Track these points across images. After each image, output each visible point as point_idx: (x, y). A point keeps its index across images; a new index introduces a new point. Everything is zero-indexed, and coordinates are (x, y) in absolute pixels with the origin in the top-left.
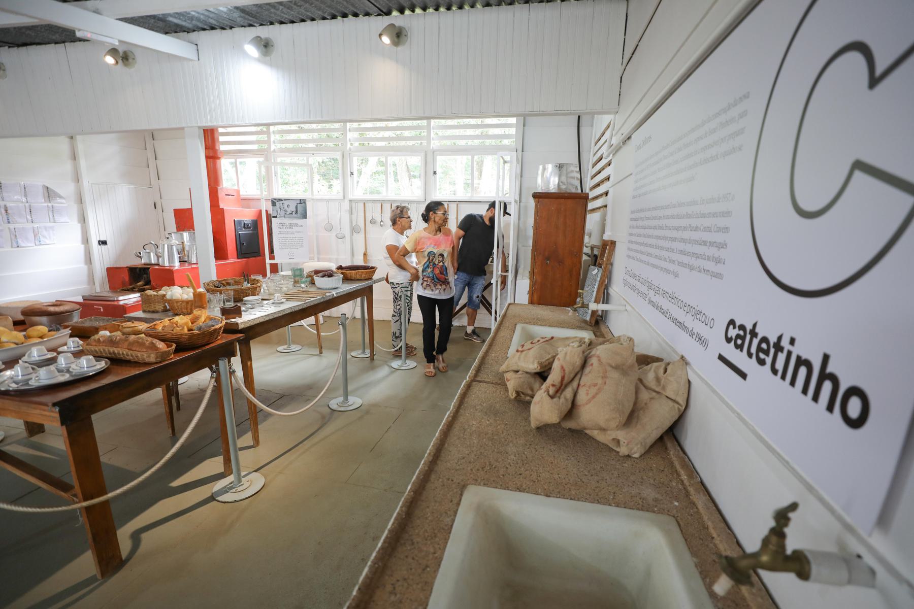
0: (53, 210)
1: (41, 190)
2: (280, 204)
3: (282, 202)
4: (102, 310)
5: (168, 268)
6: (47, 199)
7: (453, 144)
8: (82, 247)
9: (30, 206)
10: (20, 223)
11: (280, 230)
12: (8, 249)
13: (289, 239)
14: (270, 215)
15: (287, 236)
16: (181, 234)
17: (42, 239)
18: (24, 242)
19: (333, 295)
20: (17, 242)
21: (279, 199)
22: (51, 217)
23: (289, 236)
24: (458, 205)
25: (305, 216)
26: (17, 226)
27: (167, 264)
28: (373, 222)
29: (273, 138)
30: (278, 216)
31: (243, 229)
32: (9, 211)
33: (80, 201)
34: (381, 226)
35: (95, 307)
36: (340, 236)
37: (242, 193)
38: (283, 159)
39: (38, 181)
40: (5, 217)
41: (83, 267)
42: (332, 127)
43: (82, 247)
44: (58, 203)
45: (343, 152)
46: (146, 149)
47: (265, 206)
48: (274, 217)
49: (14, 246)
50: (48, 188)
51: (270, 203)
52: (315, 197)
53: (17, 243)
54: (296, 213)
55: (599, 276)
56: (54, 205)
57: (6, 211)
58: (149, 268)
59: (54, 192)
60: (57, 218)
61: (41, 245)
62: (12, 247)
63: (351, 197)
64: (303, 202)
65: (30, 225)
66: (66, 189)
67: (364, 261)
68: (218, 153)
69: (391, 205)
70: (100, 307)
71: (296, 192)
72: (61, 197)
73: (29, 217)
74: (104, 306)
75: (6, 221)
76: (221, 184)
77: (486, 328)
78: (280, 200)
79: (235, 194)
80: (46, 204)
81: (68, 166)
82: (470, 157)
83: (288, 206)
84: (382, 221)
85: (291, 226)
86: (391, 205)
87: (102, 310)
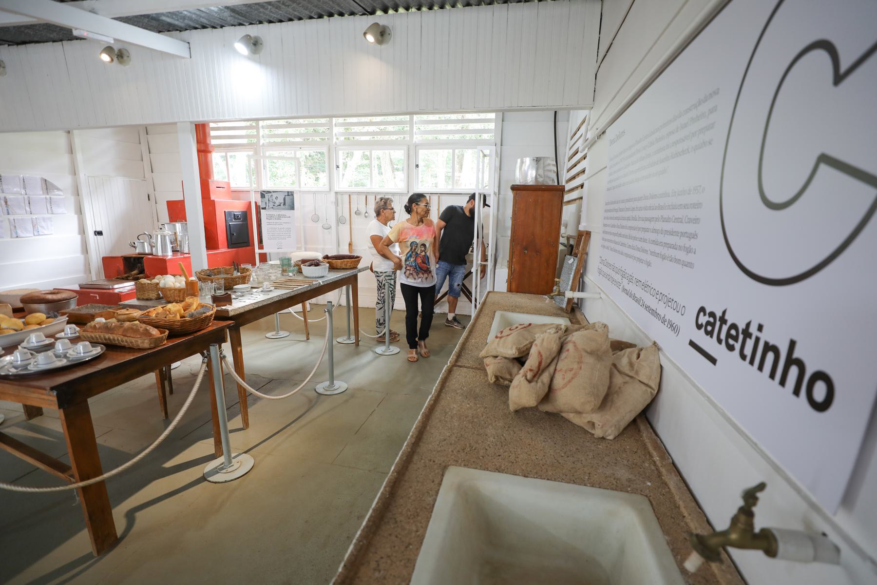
0: (50, 202)
1: (39, 183)
2: (268, 196)
3: (270, 194)
4: (98, 298)
5: (161, 257)
6: (45, 191)
8: (79, 237)
9: (29, 197)
10: (19, 214)
11: (268, 221)
13: (277, 229)
14: (259, 206)
15: (275, 226)
17: (40, 229)
18: (23, 233)
19: (320, 283)
20: (16, 233)
21: (268, 191)
22: (49, 208)
23: (277, 226)
24: (439, 197)
25: (292, 208)
26: (16, 217)
27: (160, 254)
28: (358, 213)
29: (262, 132)
31: (233, 220)
33: (77, 193)
34: (366, 217)
35: (91, 295)
36: (326, 226)
37: (232, 185)
38: (271, 152)
39: (36, 174)
40: (5, 209)
41: (80, 256)
43: (78, 238)
44: (56, 195)
45: (329, 146)
47: (254, 198)
48: (263, 208)
49: (13, 237)
50: (46, 180)
51: (259, 195)
52: (302, 189)
54: (284, 204)
55: (575, 265)
56: (52, 197)
57: (6, 202)
58: (143, 258)
59: (52, 185)
60: (55, 209)
61: (39, 235)
62: (11, 237)
63: (337, 189)
64: (290, 194)
65: (29, 217)
66: (64, 181)
67: (349, 251)
69: (376, 197)
70: (96, 295)
71: (284, 185)
72: (58, 189)
73: (28, 209)
75: (6, 212)
77: (466, 315)
78: (269, 192)
79: (225, 186)
80: (44, 196)
81: (65, 159)
82: (451, 151)
83: (276, 198)
84: (366, 212)
85: (279, 217)
86: (376, 197)
87: (98, 298)
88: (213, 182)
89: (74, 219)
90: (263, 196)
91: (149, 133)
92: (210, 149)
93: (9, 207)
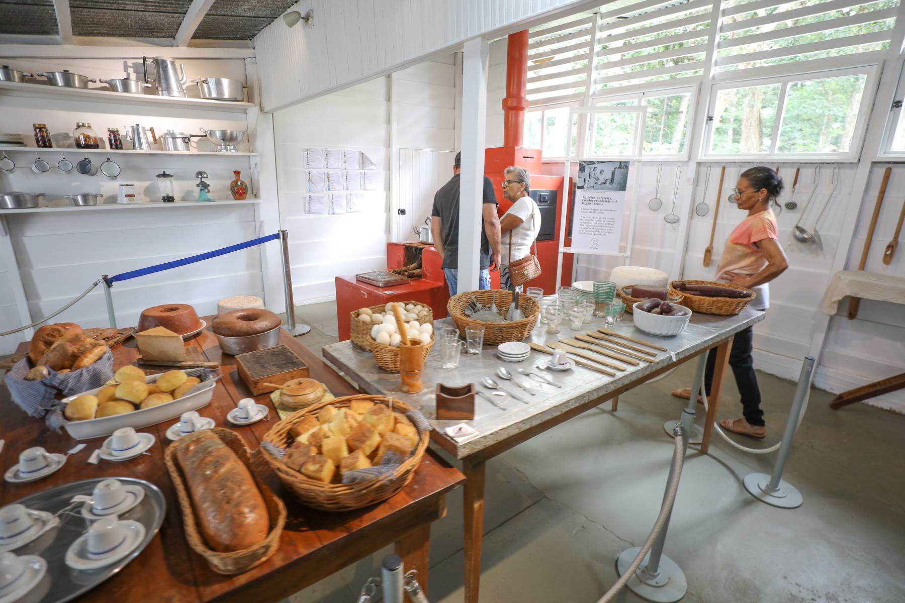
3: (593, 166)
6: (361, 165)
8: (385, 214)
9: (347, 172)
10: (338, 191)
11: (585, 206)
14: (575, 184)
15: (592, 215)
19: (671, 357)
21: (590, 162)
22: (362, 184)
25: (623, 187)
26: (352, 192)
30: (585, 186)
33: (388, 168)
36: (671, 218)
37: (543, 155)
39: (353, 148)
40: (327, 184)
42: (661, 79)
44: (370, 170)
45: (701, 83)
47: (570, 172)
48: (579, 188)
50: (363, 154)
51: (577, 168)
52: (644, 159)
54: (612, 181)
56: (366, 171)
62: (329, 214)
63: (701, 157)
64: (624, 166)
65: (345, 193)
66: (377, 156)
67: (705, 261)
71: (614, 153)
72: (372, 163)
73: (345, 184)
76: (520, 143)
78: (592, 163)
80: (359, 171)
81: (382, 131)
83: (601, 172)
85: (601, 201)
88: (520, 149)
89: (383, 194)
90: (582, 168)
92: (524, 104)
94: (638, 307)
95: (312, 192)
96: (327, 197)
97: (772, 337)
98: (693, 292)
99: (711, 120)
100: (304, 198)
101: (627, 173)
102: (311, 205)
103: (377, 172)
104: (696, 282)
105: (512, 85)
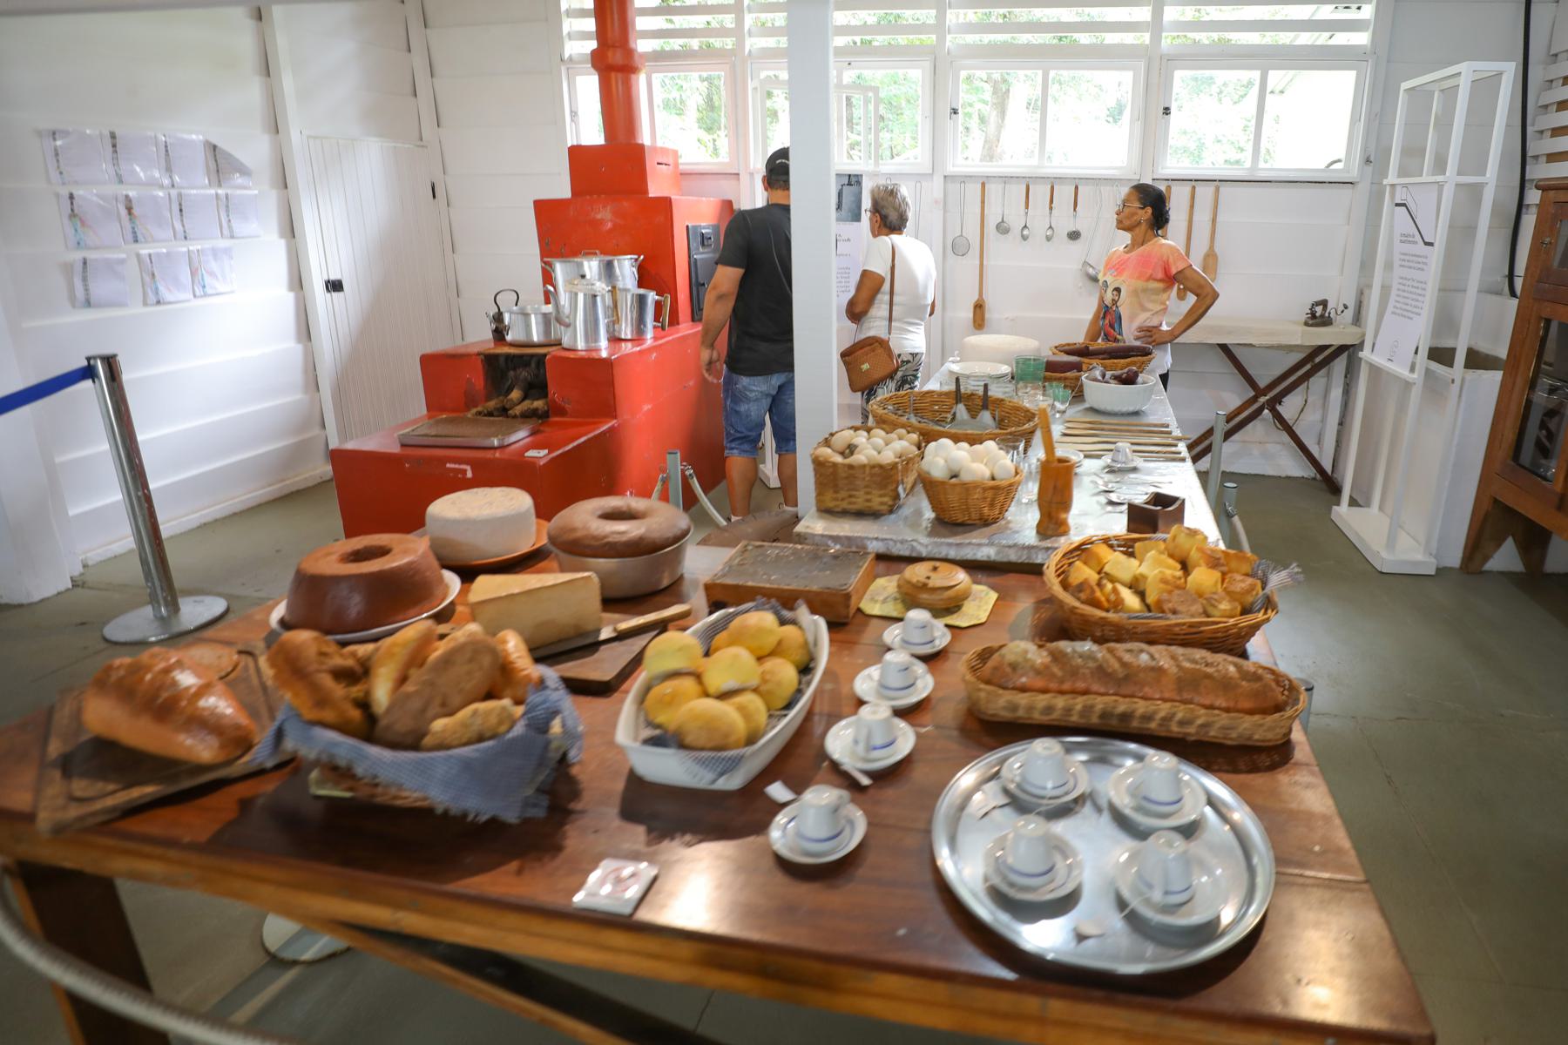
0: (227, 206)
1: (200, 156)
5: (584, 353)
6: (214, 177)
7: (852, 44)
9: (180, 195)
12: (137, 309)
16: (577, 262)
17: (208, 280)
18: (170, 290)
20: (157, 292)
24: (1194, 188)
27: (581, 345)
28: (1002, 229)
29: (749, 20)
31: (701, 250)
32: (135, 211)
33: (283, 181)
34: (1025, 238)
35: (448, 465)
39: (193, 134)
41: (289, 345)
43: (289, 298)
46: (410, 51)
49: (149, 302)
50: (215, 147)
53: (157, 293)
57: (129, 210)
58: (545, 355)
59: (228, 156)
60: (240, 227)
61: (206, 295)
62: (145, 304)
63: (951, 169)
66: (253, 150)
68: (636, 58)
69: (1077, 188)
70: (463, 467)
73: (178, 226)
74: (475, 464)
75: (130, 237)
77: (1263, 476)
79: (671, 161)
80: (213, 192)
81: (254, 91)
84: (1025, 226)
86: (1077, 188)
89: (279, 247)
91: (430, 23)
92: (637, 61)
93: (138, 222)
94: (1087, 378)
95: (88, 248)
96: (134, 261)
97: (288, 482)
98: (1101, 356)
99: (955, 113)
100: (67, 269)
101: (861, 193)
102: (91, 286)
103: (257, 191)
104: (1069, 345)
105: (609, 17)
